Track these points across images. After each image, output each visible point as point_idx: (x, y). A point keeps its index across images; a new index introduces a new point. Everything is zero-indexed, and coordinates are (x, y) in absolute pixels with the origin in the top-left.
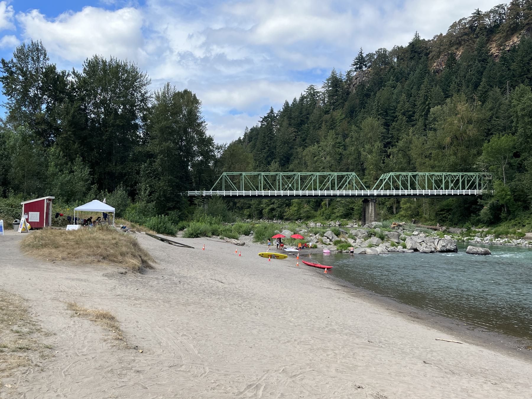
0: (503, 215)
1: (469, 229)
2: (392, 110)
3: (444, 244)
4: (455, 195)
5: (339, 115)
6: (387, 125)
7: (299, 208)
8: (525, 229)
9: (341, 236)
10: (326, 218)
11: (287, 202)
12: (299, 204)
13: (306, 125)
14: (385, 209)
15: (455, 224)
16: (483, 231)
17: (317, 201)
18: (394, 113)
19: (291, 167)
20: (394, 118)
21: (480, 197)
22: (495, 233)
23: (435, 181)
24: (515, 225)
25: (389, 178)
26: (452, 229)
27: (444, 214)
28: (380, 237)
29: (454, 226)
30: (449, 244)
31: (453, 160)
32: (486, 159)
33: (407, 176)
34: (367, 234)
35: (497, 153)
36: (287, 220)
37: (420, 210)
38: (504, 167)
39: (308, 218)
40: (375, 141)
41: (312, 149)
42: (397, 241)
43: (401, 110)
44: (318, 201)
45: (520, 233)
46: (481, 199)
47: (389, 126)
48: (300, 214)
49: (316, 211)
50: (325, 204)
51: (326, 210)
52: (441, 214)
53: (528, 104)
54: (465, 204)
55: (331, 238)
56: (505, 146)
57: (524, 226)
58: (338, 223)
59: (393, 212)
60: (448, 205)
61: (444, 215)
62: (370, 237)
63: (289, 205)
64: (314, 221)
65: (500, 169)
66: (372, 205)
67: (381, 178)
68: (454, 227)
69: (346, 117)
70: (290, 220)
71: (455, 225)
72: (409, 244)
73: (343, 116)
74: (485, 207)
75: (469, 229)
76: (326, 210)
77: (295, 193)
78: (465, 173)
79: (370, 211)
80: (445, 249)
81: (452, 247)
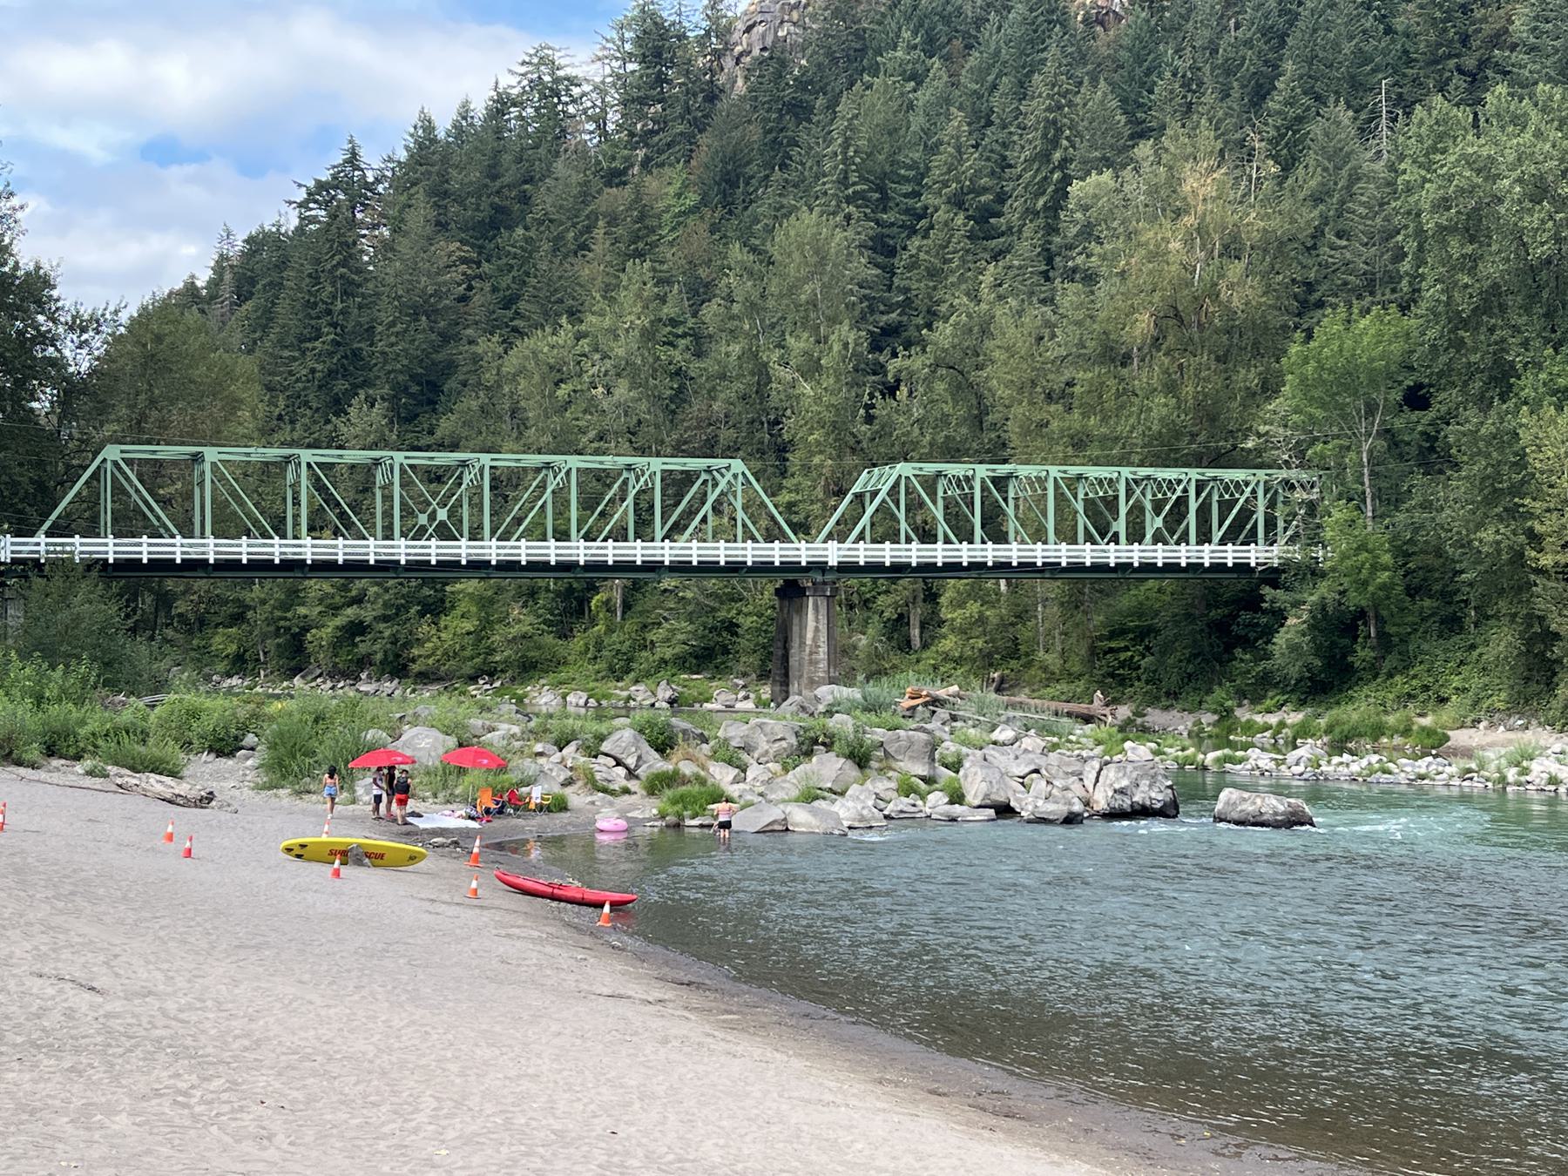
1: (1225, 715)
2: (907, 180)
3: (1125, 783)
4: (1171, 568)
5: (671, 190)
6: (883, 248)
7: (486, 625)
8: (1447, 714)
10: (612, 669)
11: (427, 591)
12: (485, 603)
13: (520, 231)
15: (1168, 694)
16: (1282, 724)
17: (570, 590)
18: (916, 195)
21: (1272, 576)
23: (1088, 503)
24: (1410, 696)
26: (1155, 717)
27: (1126, 649)
28: (851, 756)
29: (1165, 702)
30: (1144, 783)
31: (1164, 411)
35: (1340, 388)
36: (425, 678)
37: (1024, 633)
38: (1366, 447)
39: (528, 669)
40: (833, 320)
41: (548, 343)
42: (922, 770)
43: (946, 184)
44: (572, 594)
45: (1428, 732)
47: (892, 252)
48: (491, 651)
49: (564, 635)
50: (608, 605)
52: (1111, 650)
53: (1464, 183)
55: (631, 762)
56: (1371, 360)
57: (1443, 700)
58: (664, 693)
61: (1123, 656)
62: (809, 754)
63: (436, 608)
65: (1353, 455)
67: (856, 489)
68: (1166, 708)
69: (704, 202)
70: (439, 680)
71: (1170, 697)
72: (975, 784)
73: (692, 199)
74: (1291, 621)
75: (1225, 715)
78: (1211, 473)
79: (809, 635)
80: (1126, 804)
81: (1156, 795)
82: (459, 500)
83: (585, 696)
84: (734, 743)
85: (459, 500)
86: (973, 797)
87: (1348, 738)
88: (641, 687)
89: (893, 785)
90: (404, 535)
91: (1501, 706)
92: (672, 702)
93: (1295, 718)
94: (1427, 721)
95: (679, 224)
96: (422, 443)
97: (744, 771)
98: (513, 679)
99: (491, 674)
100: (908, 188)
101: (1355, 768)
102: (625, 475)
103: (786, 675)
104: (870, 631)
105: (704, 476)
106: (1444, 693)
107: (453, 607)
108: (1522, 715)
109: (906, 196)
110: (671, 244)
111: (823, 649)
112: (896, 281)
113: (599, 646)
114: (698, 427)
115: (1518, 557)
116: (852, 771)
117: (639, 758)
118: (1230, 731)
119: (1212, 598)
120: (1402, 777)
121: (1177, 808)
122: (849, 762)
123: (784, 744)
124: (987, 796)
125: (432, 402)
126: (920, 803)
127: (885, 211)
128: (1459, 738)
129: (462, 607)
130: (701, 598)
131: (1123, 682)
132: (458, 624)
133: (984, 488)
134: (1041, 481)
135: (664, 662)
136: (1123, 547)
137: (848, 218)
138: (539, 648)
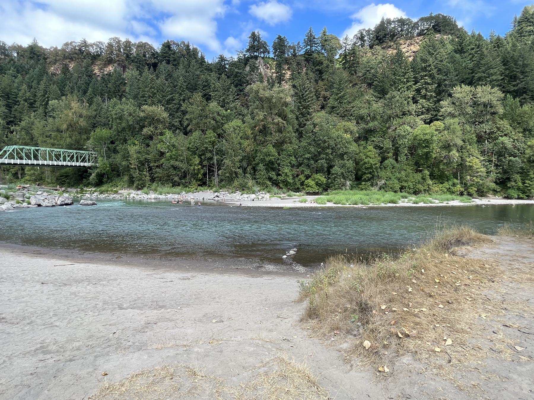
1: (82, 189)
8: (118, 188)
14: (10, 175)
21: (89, 168)
25: (13, 150)
26: (69, 189)
28: (5, 197)
35: (100, 140)
45: (115, 191)
59: (18, 178)
75: (82, 189)
80: (64, 203)
115: (128, 166)
128: (120, 192)
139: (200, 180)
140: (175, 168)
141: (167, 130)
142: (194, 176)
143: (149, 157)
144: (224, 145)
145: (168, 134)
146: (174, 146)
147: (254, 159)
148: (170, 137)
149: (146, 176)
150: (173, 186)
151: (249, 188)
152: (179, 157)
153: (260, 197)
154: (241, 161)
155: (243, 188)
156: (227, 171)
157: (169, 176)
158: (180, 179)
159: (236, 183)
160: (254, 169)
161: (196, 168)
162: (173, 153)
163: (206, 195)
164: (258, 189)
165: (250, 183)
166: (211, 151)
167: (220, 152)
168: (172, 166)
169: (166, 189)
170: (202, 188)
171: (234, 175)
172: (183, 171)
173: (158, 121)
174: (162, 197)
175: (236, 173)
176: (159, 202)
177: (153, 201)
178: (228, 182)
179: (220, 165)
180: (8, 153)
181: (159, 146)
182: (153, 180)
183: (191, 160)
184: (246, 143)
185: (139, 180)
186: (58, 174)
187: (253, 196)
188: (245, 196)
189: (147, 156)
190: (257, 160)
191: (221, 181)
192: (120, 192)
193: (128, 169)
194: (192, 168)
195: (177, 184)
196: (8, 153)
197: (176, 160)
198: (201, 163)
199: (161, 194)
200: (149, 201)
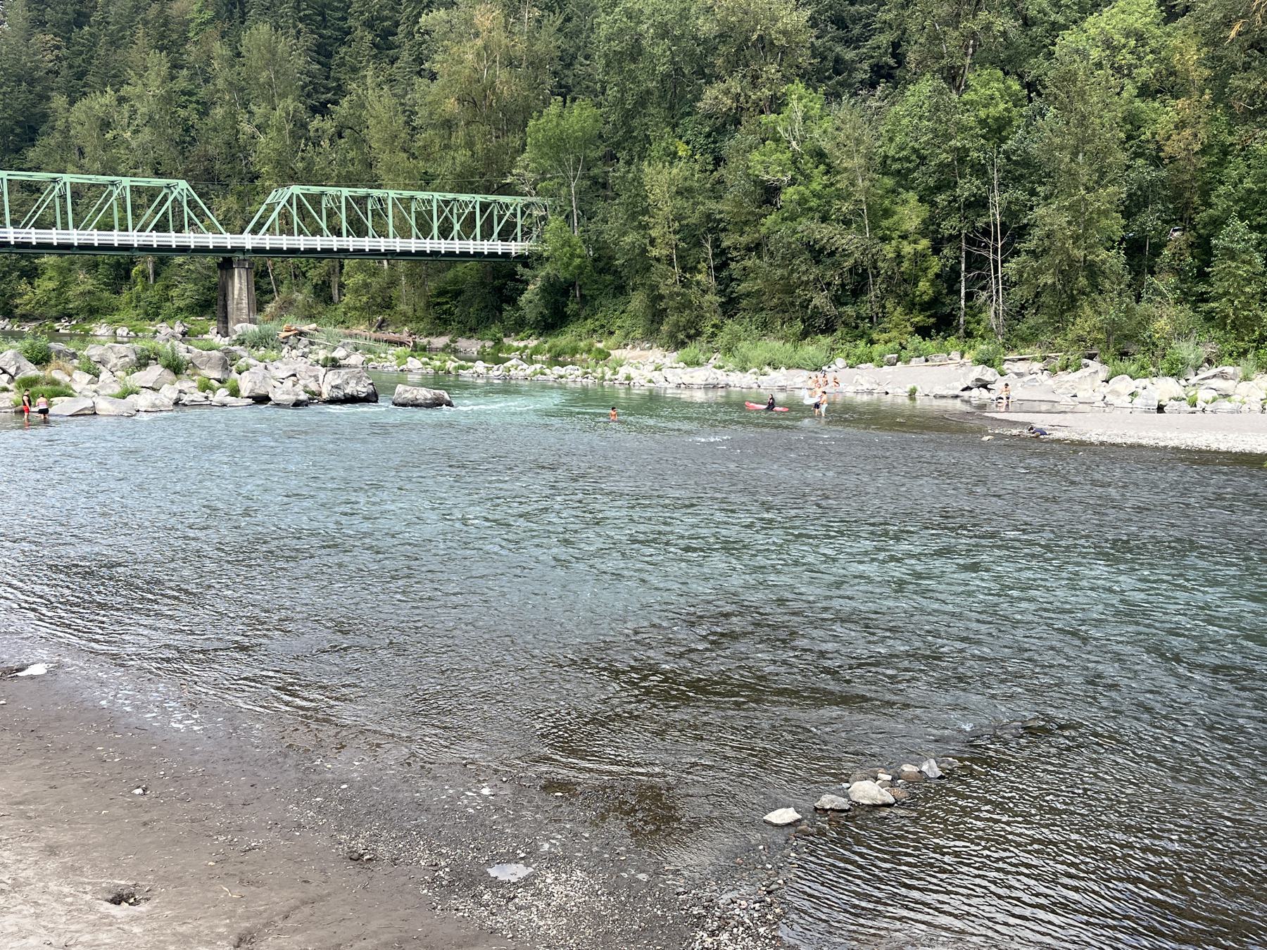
0: (570, 306)
1: (498, 342)
2: (337, 9)
3: (338, 382)
4: (478, 255)
5: (195, 8)
6: (323, 52)
7: (64, 285)
8: (612, 341)
9: (53, 365)
10: (146, 313)
11: (24, 263)
12: (62, 271)
13: (87, 28)
14: (307, 289)
15: (471, 330)
16: (526, 347)
17: (118, 263)
18: (344, 19)
19: (32, 154)
20: (344, 35)
21: (523, 259)
22: (549, 351)
23: (419, 214)
24: (595, 331)
25: (289, 201)
26: (463, 343)
27: (447, 303)
28: (168, 367)
29: (468, 334)
30: (353, 383)
31: (463, 159)
32: (533, 160)
33: (429, 201)
34: (134, 357)
35: (557, 146)
36: (26, 318)
37: (394, 293)
38: (573, 185)
39: (93, 313)
40: (283, 96)
41: (101, 102)
42: (218, 375)
43: (362, 13)
44: (119, 267)
45: (600, 351)
46: (526, 265)
47: (329, 55)
48: (68, 301)
49: (118, 292)
50: (144, 274)
51: (145, 289)
52: (438, 304)
53: (622, 26)
54: (494, 279)
55: (12, 371)
56: (574, 132)
57: (612, 333)
58: (179, 328)
59: (331, 298)
60: (455, 281)
61: (445, 307)
62: (146, 365)
63: (31, 274)
64: (110, 324)
65: (565, 189)
66: (240, 277)
67: (268, 201)
68: (469, 338)
69: (218, 15)
70: (36, 319)
71: (471, 330)
72: (246, 384)
73: (209, 14)
74: (531, 287)
75: (498, 342)
76: (145, 289)
77: (54, 236)
78: (491, 198)
79: (236, 292)
80: (340, 394)
81: (362, 389)
82: (111, 207)
83: (126, 330)
84: (94, 359)
85: (111, 207)
86: (244, 393)
87: (559, 355)
88: (164, 325)
89: (195, 384)
90: (76, 226)
91: (638, 336)
92: (184, 334)
93: (533, 343)
94: (600, 345)
95: (201, 30)
96: (25, 166)
97: (98, 376)
98: (84, 319)
99: (70, 316)
100: (339, 15)
101: (528, 372)
102: (110, 188)
103: (226, 317)
104: (305, 291)
105: (165, 191)
106: (613, 328)
107: (43, 273)
108: (648, 341)
109: (339, 19)
110: (196, 43)
111: (245, 301)
112: (332, 74)
113: (138, 299)
114: (199, 161)
115: (644, 251)
116: (169, 375)
117: (18, 368)
118: (500, 351)
119: (496, 273)
120: (551, 378)
121: (376, 396)
122: (167, 371)
123: (127, 359)
124: (252, 391)
125: (32, 140)
126: (211, 395)
127: (325, 28)
128: (616, 354)
129: (50, 273)
130: (200, 269)
131: (446, 322)
132: (46, 284)
133: (394, 204)
134: (339, 198)
135: (180, 309)
136: (478, 242)
137: (299, 32)
138: (100, 299)
139: (925, 307)
140: (817, 253)
141: (798, 88)
142: (899, 287)
143: (723, 208)
144: (1045, 134)
145: (800, 98)
146: (820, 155)
147: (1205, 193)
148: (806, 118)
149: (705, 292)
150: (804, 335)
151: (1150, 346)
152: (837, 204)
153: (1203, 395)
154: (1131, 208)
155: (1124, 346)
156: (1045, 260)
157: (789, 290)
158: (838, 301)
159: (1086, 321)
160: (1203, 249)
161: (907, 249)
162: (815, 186)
163: (934, 378)
164: (1204, 351)
165: (1164, 318)
166: (980, 170)
167: (1022, 171)
168: (809, 247)
169: (773, 346)
170: (929, 345)
171: (1083, 281)
172: (848, 264)
173: (765, 44)
174: (740, 381)
175: (1093, 271)
176: (733, 409)
177: (699, 396)
178: (1051, 314)
179: (1015, 231)
180: (278, 209)
181: (755, 156)
182: (730, 307)
183: (887, 213)
184: (1163, 117)
185: (680, 309)
186: (432, 286)
187: (1165, 388)
188: (1123, 384)
189: (712, 205)
190: (1220, 203)
191: (1018, 313)
192: (616, 354)
193: (643, 263)
194: (888, 250)
195: (820, 322)
196: (278, 209)
197: (824, 219)
198: (929, 228)
199: (744, 370)
200: (685, 395)
